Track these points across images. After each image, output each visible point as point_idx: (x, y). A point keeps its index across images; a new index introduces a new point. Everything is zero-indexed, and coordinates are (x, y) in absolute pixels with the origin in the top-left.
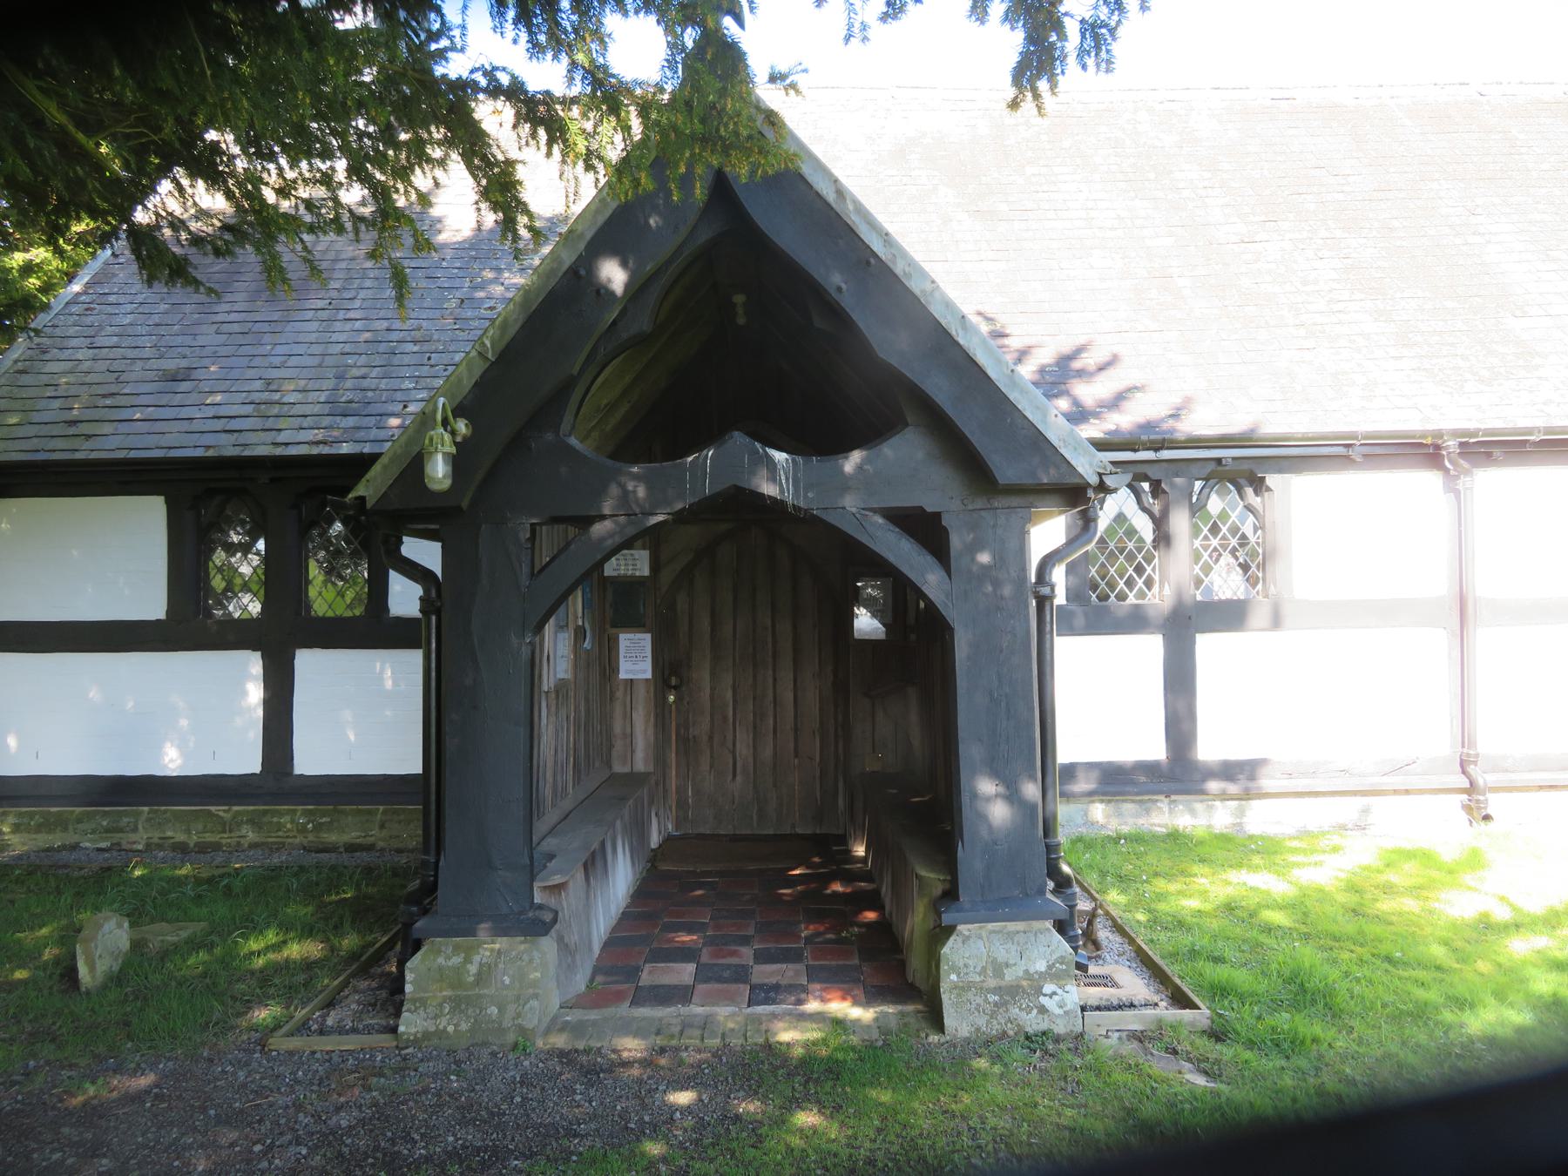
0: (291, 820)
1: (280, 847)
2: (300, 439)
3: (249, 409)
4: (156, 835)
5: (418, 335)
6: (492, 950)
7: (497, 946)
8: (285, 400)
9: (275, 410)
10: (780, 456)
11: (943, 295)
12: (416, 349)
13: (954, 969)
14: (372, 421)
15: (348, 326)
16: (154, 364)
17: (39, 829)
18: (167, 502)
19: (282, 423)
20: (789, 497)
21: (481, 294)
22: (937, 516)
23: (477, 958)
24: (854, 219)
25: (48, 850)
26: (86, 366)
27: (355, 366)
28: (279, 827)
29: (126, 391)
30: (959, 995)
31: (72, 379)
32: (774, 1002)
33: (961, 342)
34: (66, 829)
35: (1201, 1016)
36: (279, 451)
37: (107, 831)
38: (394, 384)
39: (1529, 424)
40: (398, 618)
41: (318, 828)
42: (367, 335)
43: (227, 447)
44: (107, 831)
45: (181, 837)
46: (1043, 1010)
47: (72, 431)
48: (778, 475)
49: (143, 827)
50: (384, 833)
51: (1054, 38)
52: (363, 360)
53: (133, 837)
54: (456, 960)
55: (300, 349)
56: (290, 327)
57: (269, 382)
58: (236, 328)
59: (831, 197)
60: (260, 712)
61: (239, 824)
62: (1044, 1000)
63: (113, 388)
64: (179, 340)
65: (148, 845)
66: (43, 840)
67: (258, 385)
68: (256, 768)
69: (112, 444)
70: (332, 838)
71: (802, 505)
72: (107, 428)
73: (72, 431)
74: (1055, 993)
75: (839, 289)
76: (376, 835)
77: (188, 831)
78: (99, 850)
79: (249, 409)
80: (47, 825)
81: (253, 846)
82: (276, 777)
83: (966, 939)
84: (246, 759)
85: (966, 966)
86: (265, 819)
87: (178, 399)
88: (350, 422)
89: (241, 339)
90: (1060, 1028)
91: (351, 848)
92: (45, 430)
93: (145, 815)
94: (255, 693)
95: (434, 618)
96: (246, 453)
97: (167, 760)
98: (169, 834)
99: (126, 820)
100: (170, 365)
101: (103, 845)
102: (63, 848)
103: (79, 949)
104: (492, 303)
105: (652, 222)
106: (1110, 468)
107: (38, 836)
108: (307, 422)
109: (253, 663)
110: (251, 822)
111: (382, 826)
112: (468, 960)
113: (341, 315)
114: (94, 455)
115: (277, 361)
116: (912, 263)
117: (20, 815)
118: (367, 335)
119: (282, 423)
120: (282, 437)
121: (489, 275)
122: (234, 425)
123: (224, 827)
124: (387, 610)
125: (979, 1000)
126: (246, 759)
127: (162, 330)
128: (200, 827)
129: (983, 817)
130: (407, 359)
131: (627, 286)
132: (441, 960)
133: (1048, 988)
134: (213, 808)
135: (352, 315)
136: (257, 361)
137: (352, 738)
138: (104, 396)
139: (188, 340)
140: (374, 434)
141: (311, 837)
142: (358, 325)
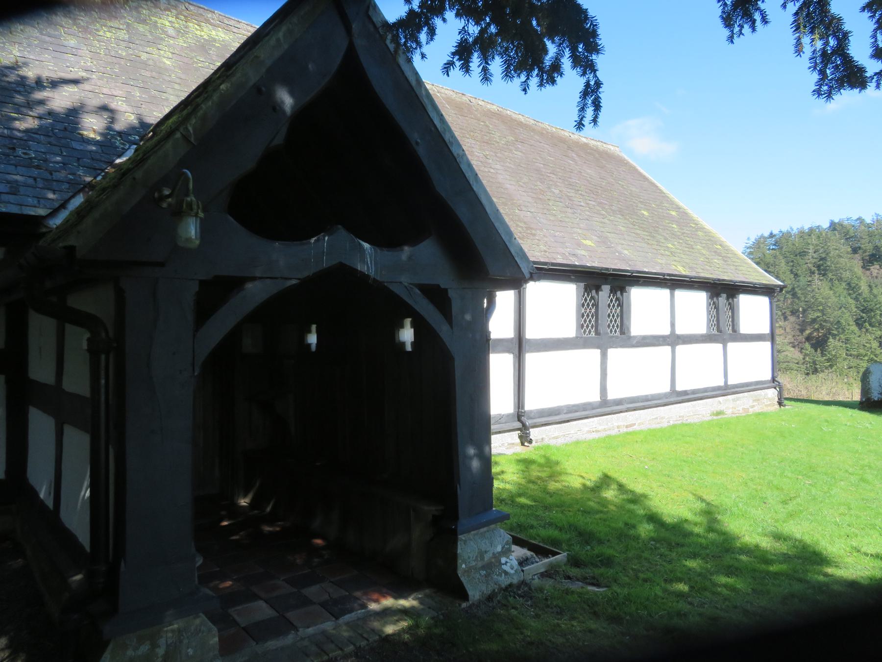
6: (173, 631)
7: (176, 626)
10: (366, 245)
11: (467, 159)
13: (464, 562)
20: (372, 273)
22: (446, 290)
23: (162, 642)
24: (425, 101)
30: (469, 576)
32: (351, 611)
33: (475, 189)
35: (562, 557)
39: (546, 260)
46: (506, 573)
48: (368, 259)
54: (144, 648)
59: (414, 83)
62: (504, 567)
71: (378, 279)
74: (507, 562)
75: (417, 143)
83: (465, 542)
85: (469, 558)
90: (515, 581)
95: (103, 357)
105: (310, 66)
106: (535, 271)
112: (154, 645)
116: (453, 136)
125: (478, 576)
129: (469, 469)
131: (293, 108)
132: (130, 653)
133: (503, 560)
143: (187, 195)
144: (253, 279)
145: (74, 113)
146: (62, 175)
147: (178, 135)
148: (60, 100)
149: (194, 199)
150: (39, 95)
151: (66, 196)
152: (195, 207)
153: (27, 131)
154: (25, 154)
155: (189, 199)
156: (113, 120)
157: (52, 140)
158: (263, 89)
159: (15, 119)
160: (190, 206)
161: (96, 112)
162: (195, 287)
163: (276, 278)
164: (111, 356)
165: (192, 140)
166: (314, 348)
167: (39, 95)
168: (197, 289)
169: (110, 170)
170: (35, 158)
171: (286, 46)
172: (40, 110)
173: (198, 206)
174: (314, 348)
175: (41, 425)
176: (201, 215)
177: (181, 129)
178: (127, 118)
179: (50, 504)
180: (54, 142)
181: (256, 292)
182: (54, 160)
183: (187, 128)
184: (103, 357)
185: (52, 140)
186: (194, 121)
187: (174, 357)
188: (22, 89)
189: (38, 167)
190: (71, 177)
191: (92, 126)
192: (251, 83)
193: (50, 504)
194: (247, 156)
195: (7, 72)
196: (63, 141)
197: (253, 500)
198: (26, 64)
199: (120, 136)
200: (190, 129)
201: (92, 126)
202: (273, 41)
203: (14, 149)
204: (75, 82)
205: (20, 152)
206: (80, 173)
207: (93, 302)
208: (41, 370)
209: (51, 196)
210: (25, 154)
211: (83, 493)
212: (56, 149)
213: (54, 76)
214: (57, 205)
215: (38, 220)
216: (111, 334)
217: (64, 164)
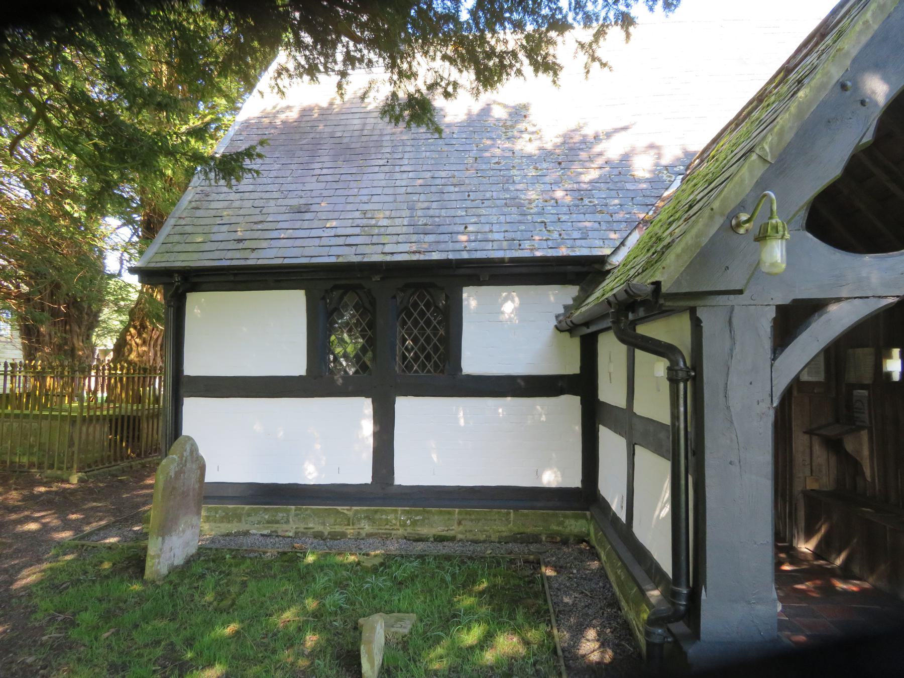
0: (397, 519)
1: (387, 537)
2: (400, 249)
3: (357, 231)
4: (301, 527)
5: (455, 181)
8: (380, 224)
9: (376, 231)
12: (457, 189)
14: (446, 237)
15: (405, 176)
16: (280, 202)
17: (222, 520)
18: (307, 295)
19: (384, 239)
21: (487, 154)
22: (779, 308)
25: (228, 535)
26: (237, 204)
27: (419, 201)
28: (387, 522)
29: (269, 219)
31: (230, 212)
34: (240, 521)
36: (388, 258)
37: (268, 522)
38: (452, 213)
40: (468, 376)
41: (414, 523)
42: (420, 182)
43: (350, 256)
44: (268, 522)
45: (319, 528)
47: (241, 246)
49: (292, 522)
50: (461, 528)
51: (496, 78)
52: (422, 198)
53: (285, 527)
55: (379, 191)
56: (365, 177)
57: (365, 212)
58: (329, 178)
60: (371, 441)
61: (359, 520)
63: (260, 218)
64: (293, 187)
65: (296, 533)
66: (225, 528)
67: (357, 214)
68: (369, 480)
69: (270, 254)
70: (424, 531)
72: (264, 244)
73: (241, 246)
76: (454, 530)
77: (324, 524)
78: (262, 535)
79: (357, 231)
80: (227, 518)
81: (369, 535)
82: (382, 490)
84: (361, 473)
86: (377, 516)
87: (306, 224)
88: (431, 238)
89: (335, 186)
91: (440, 539)
92: (222, 246)
93: (293, 512)
94: (368, 427)
95: (682, 385)
96: (366, 260)
97: (307, 473)
98: (311, 525)
99: (281, 515)
100: (295, 202)
101: (265, 532)
102: (238, 534)
103: (362, 648)
104: (496, 160)
107: (222, 525)
108: (401, 238)
109: (364, 406)
110: (367, 518)
111: (460, 523)
113: (397, 169)
114: (260, 262)
115: (365, 199)
117: (208, 510)
118: (420, 182)
119: (384, 239)
120: (387, 249)
121: (489, 142)
122: (350, 241)
123: (349, 522)
124: (461, 370)
126: (361, 473)
127: (281, 181)
128: (332, 521)
130: (453, 197)
134: (339, 508)
135: (403, 169)
136: (351, 199)
137: (435, 459)
138: (255, 223)
139: (300, 187)
140: (451, 246)
141: (409, 530)
142: (411, 175)
143: (771, 218)
144: (838, 300)
145: (626, 158)
146: (620, 216)
147: (754, 157)
148: (613, 149)
149: (779, 221)
150: (597, 149)
151: (625, 235)
152: (780, 228)
153: (590, 182)
154: (590, 202)
155: (774, 221)
156: (659, 156)
157: (610, 186)
158: (849, 84)
159: (581, 174)
160: (776, 229)
161: (644, 152)
162: (772, 313)
163: (867, 297)
164: (689, 383)
165: (769, 159)
166: (896, 377)
167: (597, 149)
168: (774, 316)
169: (660, 204)
170: (598, 205)
171: (876, 27)
172: (600, 161)
173: (784, 227)
174: (896, 377)
175: (611, 444)
176: (787, 236)
177: (757, 150)
178: (671, 154)
179: (623, 517)
180: (612, 187)
181: (840, 318)
182: (613, 203)
183: (763, 148)
184: (682, 385)
185: (609, 185)
186: (770, 138)
187: (750, 386)
188: (584, 146)
189: (601, 212)
190: (628, 216)
191: (642, 167)
192: (834, 81)
193: (623, 517)
194: (829, 164)
195: (572, 134)
196: (619, 185)
197: (818, 546)
198: (586, 124)
199: (667, 170)
200: (767, 147)
201: (642, 167)
202: (859, 26)
203: (582, 199)
204: (625, 129)
205: (586, 201)
206: (635, 211)
207: (671, 330)
208: (611, 392)
209: (612, 235)
210: (590, 202)
211: (657, 513)
212: (613, 193)
213: (609, 128)
214: (618, 243)
215: (602, 260)
216: (688, 364)
217: (621, 205)
